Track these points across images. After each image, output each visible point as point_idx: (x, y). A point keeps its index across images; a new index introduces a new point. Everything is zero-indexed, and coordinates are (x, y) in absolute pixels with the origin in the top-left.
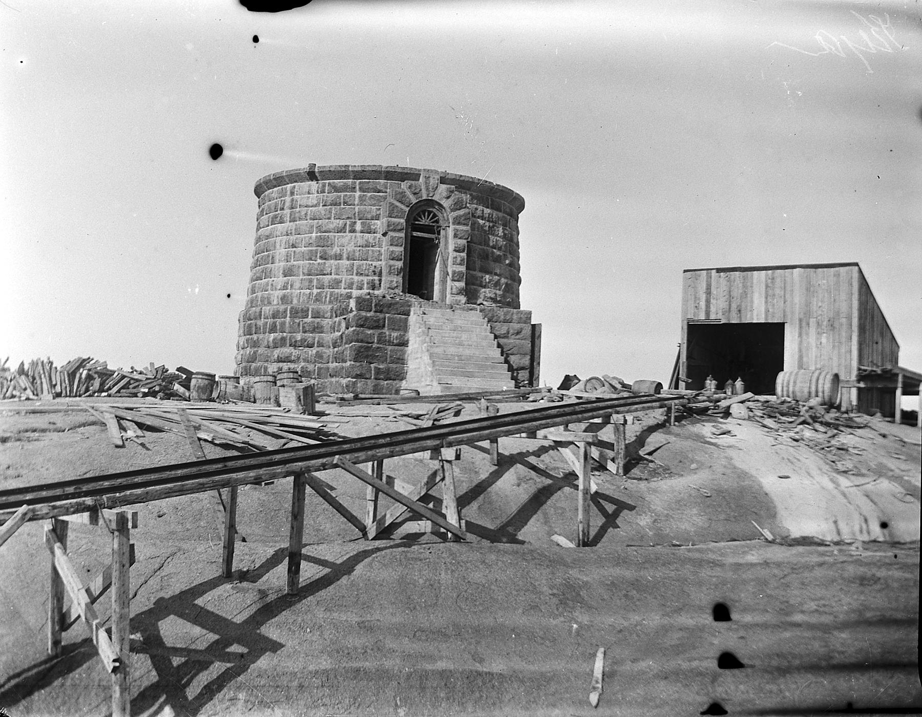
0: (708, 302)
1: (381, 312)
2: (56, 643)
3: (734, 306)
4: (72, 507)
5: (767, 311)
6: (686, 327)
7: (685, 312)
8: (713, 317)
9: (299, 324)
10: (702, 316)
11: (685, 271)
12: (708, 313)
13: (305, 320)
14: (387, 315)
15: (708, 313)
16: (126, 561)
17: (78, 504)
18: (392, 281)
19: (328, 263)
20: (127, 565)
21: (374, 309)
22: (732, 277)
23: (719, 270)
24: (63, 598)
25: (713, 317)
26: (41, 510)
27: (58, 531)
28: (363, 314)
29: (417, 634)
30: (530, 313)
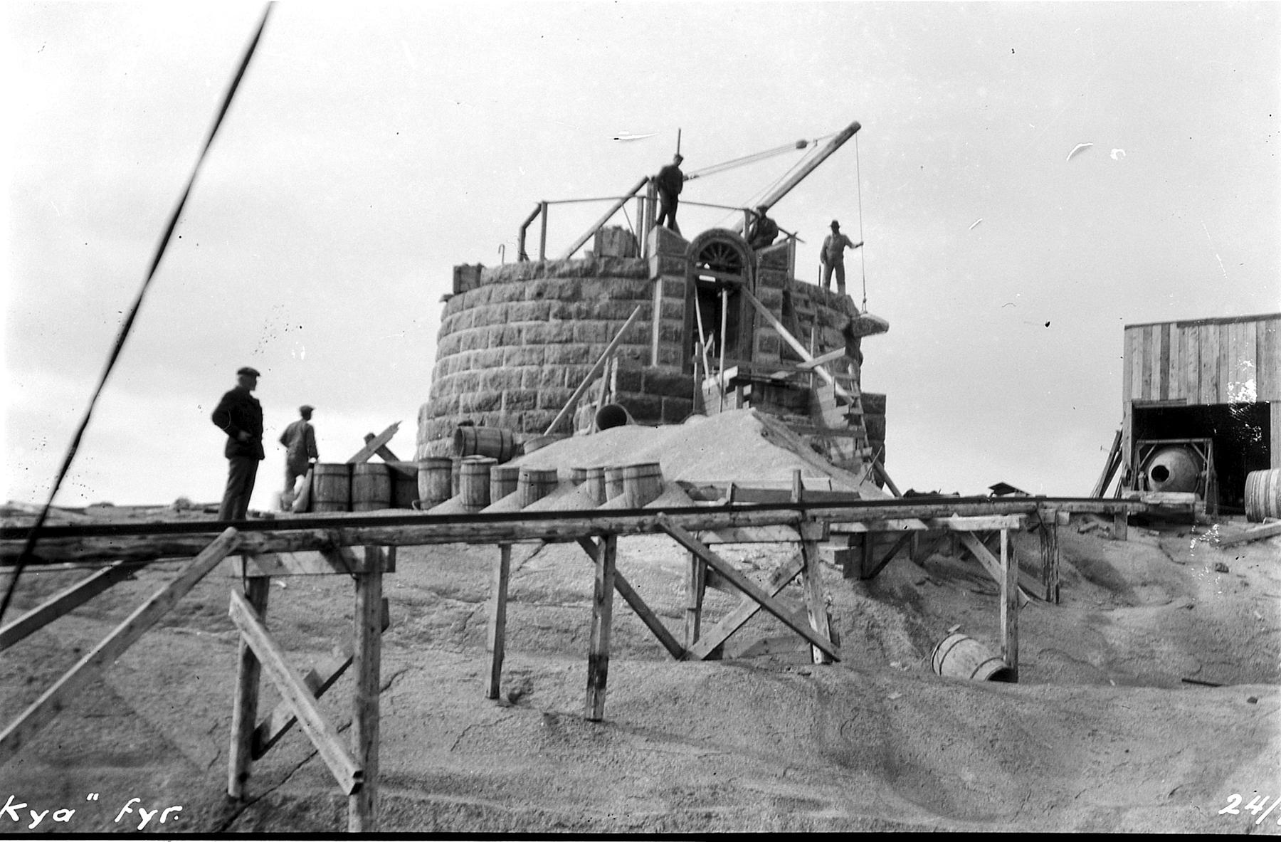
0: (1165, 372)
1: (654, 392)
2: (243, 777)
3: (1206, 377)
4: (296, 539)
5: (1026, 665)
6: (1129, 412)
7: (1128, 388)
8: (1173, 396)
9: (520, 419)
10: (1156, 396)
11: (1127, 328)
12: (1164, 389)
13: (531, 412)
14: (664, 398)
15: (1164, 389)
16: (376, 622)
17: (307, 537)
18: (667, 352)
19: (568, 324)
20: (378, 630)
21: (643, 389)
22: (1203, 335)
23: (1181, 325)
24: (256, 705)
25: (1173, 396)
26: (252, 538)
27: (255, 598)
28: (628, 395)
29: (789, 773)
30: (883, 398)
